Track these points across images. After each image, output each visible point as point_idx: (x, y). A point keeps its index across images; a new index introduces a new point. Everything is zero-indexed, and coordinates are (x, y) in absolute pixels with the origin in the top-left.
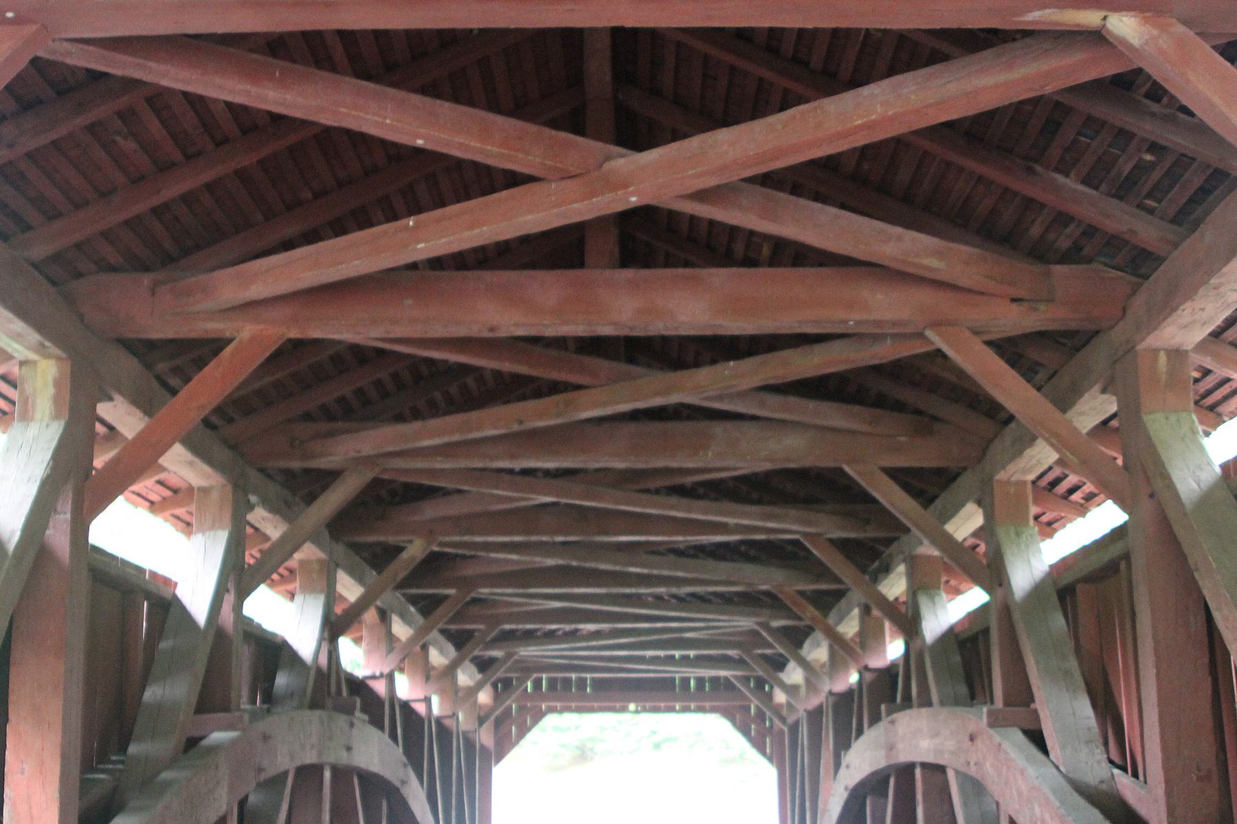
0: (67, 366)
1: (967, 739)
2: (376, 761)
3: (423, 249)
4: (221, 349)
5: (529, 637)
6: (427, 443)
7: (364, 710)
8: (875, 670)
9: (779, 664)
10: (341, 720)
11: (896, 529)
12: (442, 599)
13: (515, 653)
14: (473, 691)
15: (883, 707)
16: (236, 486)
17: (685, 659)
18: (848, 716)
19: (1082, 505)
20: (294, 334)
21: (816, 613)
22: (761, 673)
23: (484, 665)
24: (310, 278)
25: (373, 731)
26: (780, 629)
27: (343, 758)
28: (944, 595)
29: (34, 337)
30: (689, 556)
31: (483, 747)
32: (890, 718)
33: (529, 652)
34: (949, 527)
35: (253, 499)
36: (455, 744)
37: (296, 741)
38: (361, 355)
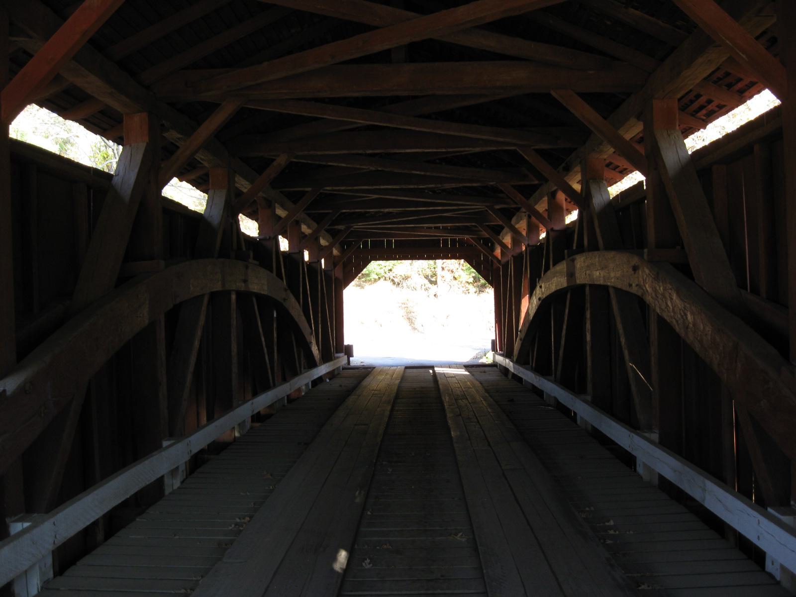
1: (631, 270)
2: (265, 288)
4: (529, 313)
5: (362, 217)
7: (254, 259)
8: (557, 231)
9: (498, 230)
11: (583, 134)
12: (303, 193)
13: (352, 227)
14: (329, 248)
15: (566, 251)
17: (445, 228)
18: (538, 261)
19: (703, 120)
21: (523, 198)
22: (487, 236)
23: (333, 234)
25: (263, 272)
26: (500, 210)
27: (242, 287)
31: (336, 279)
32: (571, 258)
33: (358, 226)
34: (621, 132)
36: (319, 278)
37: (202, 279)
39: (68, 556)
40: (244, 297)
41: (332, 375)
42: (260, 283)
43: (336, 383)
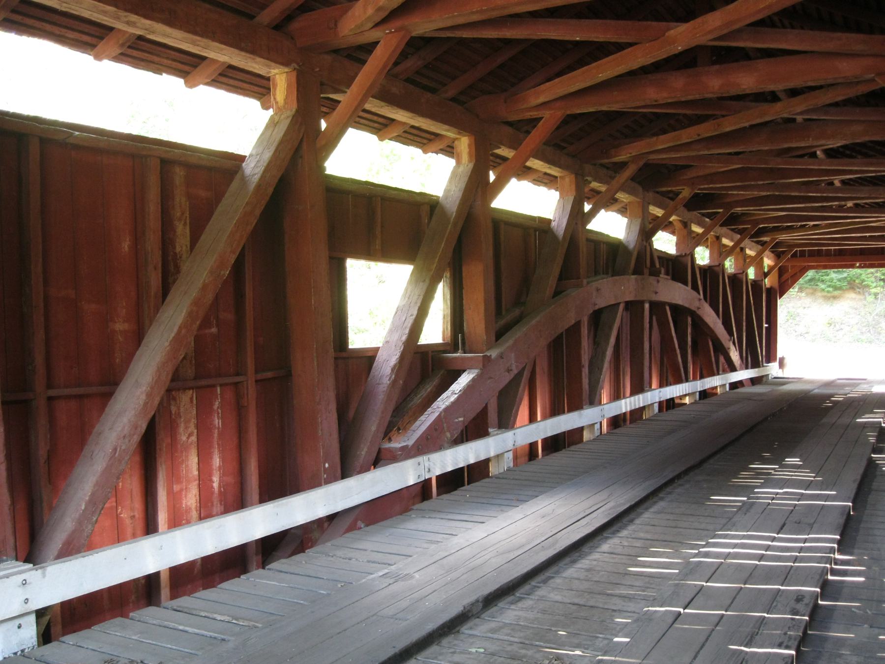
0: (473, 138)
3: (602, 76)
6: (660, 147)
7: (667, 274)
10: (652, 279)
16: (577, 174)
20: (569, 112)
24: (621, 69)
28: (631, 246)
29: (455, 130)
30: (850, 185)
35: (589, 179)
37: (612, 291)
38: (619, 114)
39: (61, 621)
40: (657, 307)
41: (754, 381)
42: (678, 294)
43: (758, 389)
